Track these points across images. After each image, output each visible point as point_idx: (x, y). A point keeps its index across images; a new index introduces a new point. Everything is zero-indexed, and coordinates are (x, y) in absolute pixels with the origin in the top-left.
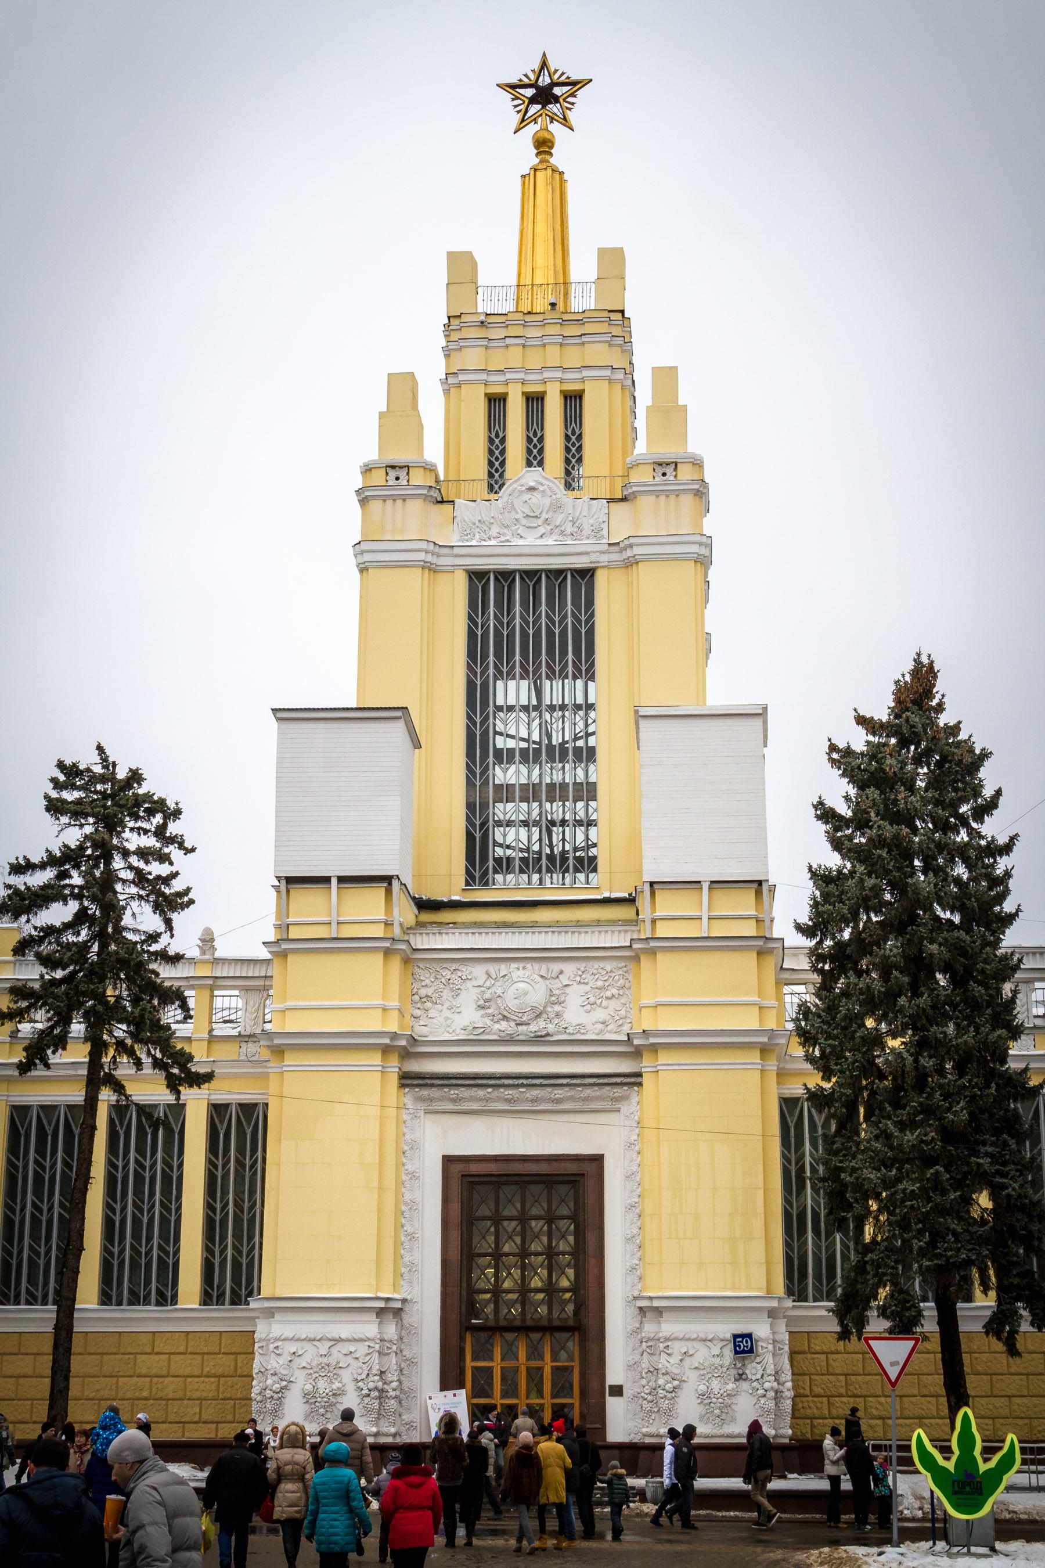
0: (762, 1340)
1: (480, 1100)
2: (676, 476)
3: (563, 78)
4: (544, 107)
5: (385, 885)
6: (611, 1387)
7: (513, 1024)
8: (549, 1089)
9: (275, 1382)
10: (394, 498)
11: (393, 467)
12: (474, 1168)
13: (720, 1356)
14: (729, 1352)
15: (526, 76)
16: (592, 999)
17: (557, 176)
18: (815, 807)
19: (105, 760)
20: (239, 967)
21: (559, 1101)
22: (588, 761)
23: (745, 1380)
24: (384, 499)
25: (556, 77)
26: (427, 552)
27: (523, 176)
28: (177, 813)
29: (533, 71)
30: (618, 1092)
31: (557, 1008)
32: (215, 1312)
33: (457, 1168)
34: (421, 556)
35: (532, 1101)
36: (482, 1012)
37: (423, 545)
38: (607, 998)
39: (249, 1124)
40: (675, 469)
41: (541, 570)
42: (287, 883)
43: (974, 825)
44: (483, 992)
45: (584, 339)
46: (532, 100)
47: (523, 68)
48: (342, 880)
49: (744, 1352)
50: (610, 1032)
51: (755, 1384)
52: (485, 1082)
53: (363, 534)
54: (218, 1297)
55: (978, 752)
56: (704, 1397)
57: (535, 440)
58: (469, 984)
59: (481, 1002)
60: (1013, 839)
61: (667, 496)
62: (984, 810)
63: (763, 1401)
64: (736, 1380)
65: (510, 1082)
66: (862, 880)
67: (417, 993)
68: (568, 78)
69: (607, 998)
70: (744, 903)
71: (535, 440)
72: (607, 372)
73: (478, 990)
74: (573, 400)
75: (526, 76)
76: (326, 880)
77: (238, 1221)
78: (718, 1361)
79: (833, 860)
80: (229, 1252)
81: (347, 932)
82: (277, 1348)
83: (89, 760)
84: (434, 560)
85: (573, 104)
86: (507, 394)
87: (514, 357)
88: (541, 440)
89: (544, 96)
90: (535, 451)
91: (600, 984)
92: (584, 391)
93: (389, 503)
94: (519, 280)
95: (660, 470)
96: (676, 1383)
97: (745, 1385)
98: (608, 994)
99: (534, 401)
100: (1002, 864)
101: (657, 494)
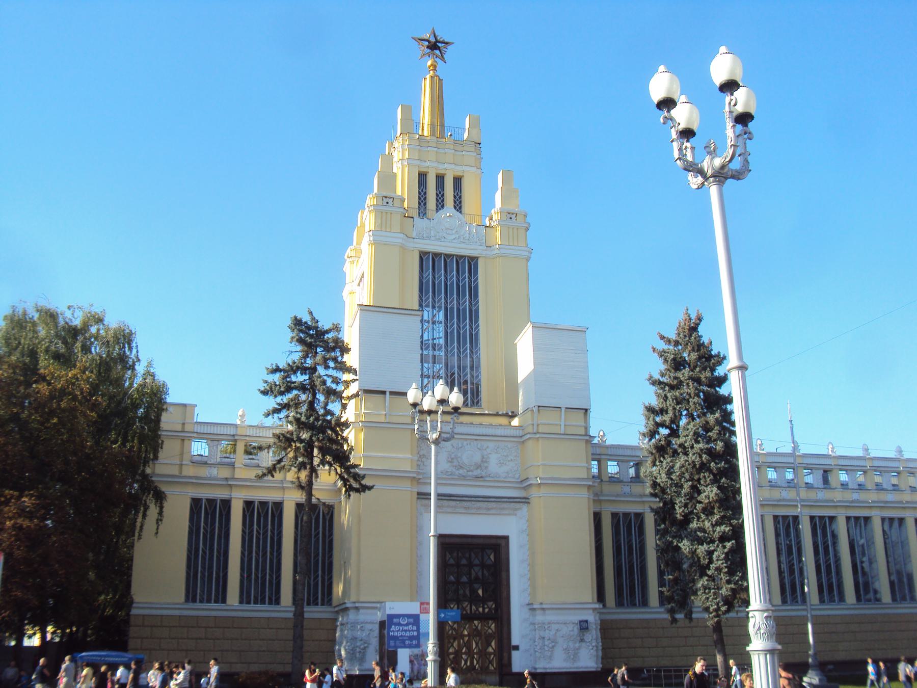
1: (452, 507)
7: (465, 471)
9: (361, 644)
11: (386, 197)
13: (573, 631)
14: (576, 629)
16: (502, 461)
18: (649, 380)
19: (313, 319)
21: (489, 509)
23: (584, 641)
30: (518, 506)
31: (486, 464)
32: (245, 607)
33: (503, 542)
39: (314, 514)
40: (516, 217)
41: (454, 255)
48: (392, 393)
49: (584, 629)
50: (510, 477)
51: (588, 644)
52: (455, 498)
54: (275, 600)
55: (722, 356)
56: (566, 650)
57: (422, 193)
59: (450, 459)
64: (580, 642)
70: (579, 416)
74: (458, 181)
76: (384, 393)
78: (572, 633)
82: (362, 627)
83: (306, 318)
90: (440, 201)
91: (505, 454)
92: (463, 176)
95: (509, 216)
96: (553, 644)
97: (583, 644)
98: (509, 459)
99: (440, 179)
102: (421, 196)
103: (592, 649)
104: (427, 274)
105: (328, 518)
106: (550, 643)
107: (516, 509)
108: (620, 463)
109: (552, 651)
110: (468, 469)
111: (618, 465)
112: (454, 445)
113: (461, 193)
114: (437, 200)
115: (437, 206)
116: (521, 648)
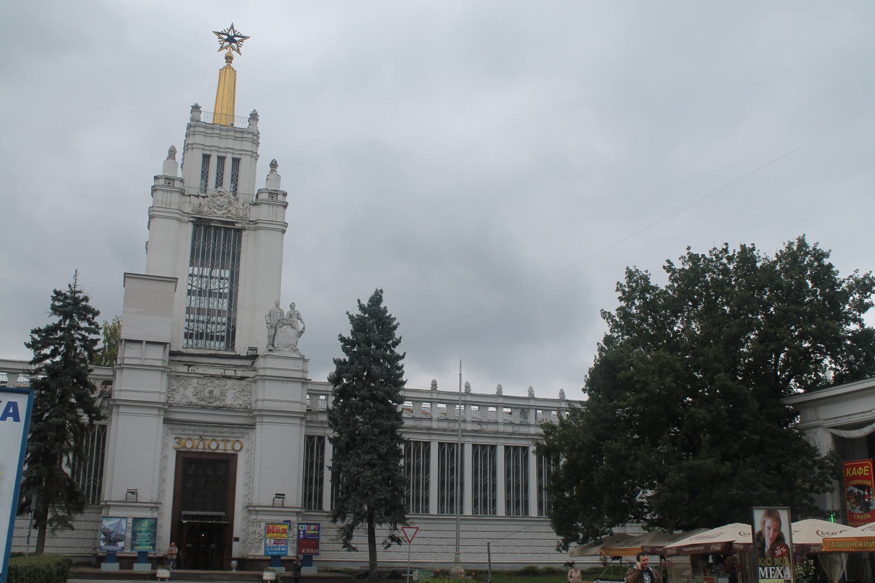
0: (294, 523)
2: (277, 199)
3: (238, 34)
4: (230, 44)
5: (164, 346)
6: (235, 538)
7: (206, 402)
8: (220, 428)
10: (167, 191)
12: (188, 456)
15: (225, 30)
16: (237, 396)
17: (234, 72)
20: (99, 370)
21: (223, 433)
22: (219, 298)
24: (163, 191)
25: (236, 33)
26: (179, 214)
27: (220, 69)
28: (97, 313)
29: (228, 29)
30: (246, 431)
31: (223, 398)
34: (176, 216)
35: (213, 432)
36: (195, 397)
37: (178, 211)
38: (243, 396)
40: (277, 196)
42: (125, 342)
43: (392, 349)
44: (196, 390)
45: (243, 139)
46: (226, 40)
47: (223, 27)
48: (147, 342)
53: (153, 205)
57: (220, 174)
58: (190, 385)
59: (195, 393)
60: (404, 354)
61: (273, 206)
62: (396, 344)
63: (292, 544)
65: (205, 424)
66: (357, 366)
67: (170, 388)
68: (241, 34)
69: (243, 396)
71: (220, 174)
72: (251, 153)
73: (194, 389)
74: (236, 162)
75: (225, 30)
76: (141, 342)
77: (96, 470)
79: (344, 357)
80: (92, 482)
81: (147, 363)
84: (181, 217)
85: (242, 45)
86: (226, 157)
87: (215, 141)
88: (222, 174)
89: (231, 40)
92: (211, 155)
93: (165, 193)
94: (215, 110)
99: (221, 160)
100: (400, 363)
101: (269, 204)
102: (203, 175)
103: (293, 543)
104: (198, 242)
105: (102, 435)
106: (259, 537)
107: (245, 434)
108: (414, 403)
109: (260, 543)
110: (209, 401)
111: (412, 404)
112: (199, 382)
113: (223, 171)
114: (217, 178)
115: (217, 183)
116: (240, 540)
